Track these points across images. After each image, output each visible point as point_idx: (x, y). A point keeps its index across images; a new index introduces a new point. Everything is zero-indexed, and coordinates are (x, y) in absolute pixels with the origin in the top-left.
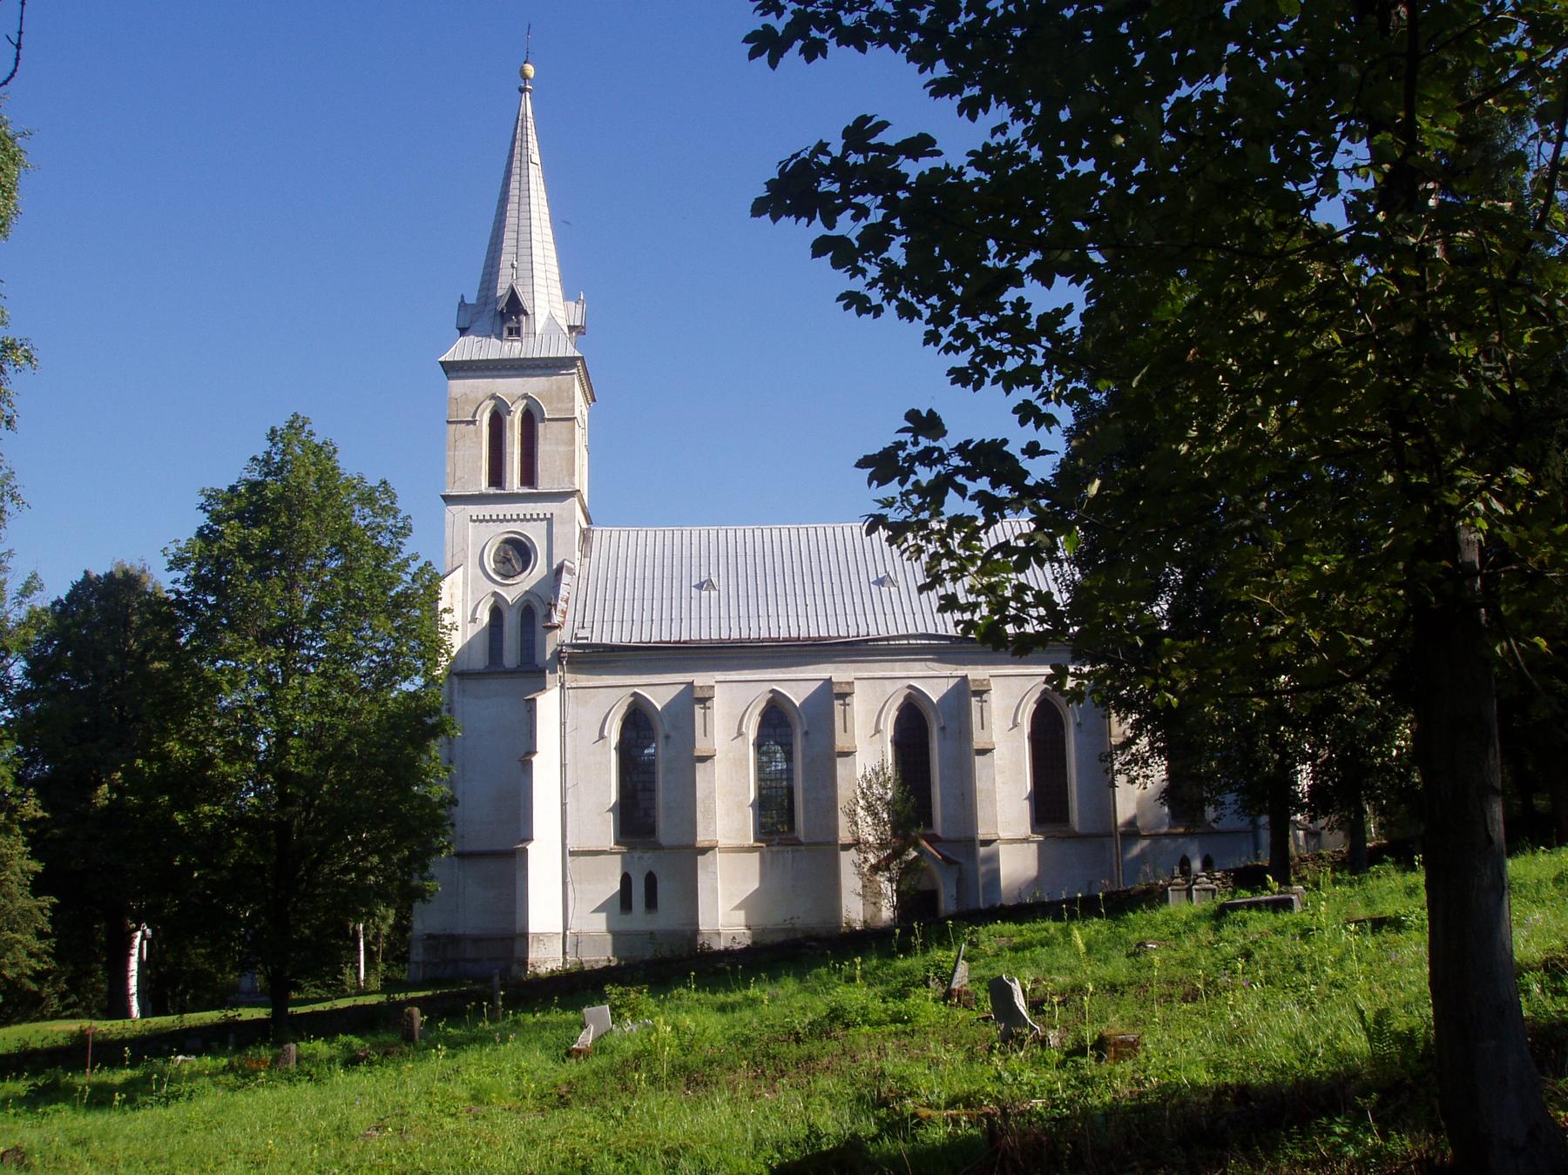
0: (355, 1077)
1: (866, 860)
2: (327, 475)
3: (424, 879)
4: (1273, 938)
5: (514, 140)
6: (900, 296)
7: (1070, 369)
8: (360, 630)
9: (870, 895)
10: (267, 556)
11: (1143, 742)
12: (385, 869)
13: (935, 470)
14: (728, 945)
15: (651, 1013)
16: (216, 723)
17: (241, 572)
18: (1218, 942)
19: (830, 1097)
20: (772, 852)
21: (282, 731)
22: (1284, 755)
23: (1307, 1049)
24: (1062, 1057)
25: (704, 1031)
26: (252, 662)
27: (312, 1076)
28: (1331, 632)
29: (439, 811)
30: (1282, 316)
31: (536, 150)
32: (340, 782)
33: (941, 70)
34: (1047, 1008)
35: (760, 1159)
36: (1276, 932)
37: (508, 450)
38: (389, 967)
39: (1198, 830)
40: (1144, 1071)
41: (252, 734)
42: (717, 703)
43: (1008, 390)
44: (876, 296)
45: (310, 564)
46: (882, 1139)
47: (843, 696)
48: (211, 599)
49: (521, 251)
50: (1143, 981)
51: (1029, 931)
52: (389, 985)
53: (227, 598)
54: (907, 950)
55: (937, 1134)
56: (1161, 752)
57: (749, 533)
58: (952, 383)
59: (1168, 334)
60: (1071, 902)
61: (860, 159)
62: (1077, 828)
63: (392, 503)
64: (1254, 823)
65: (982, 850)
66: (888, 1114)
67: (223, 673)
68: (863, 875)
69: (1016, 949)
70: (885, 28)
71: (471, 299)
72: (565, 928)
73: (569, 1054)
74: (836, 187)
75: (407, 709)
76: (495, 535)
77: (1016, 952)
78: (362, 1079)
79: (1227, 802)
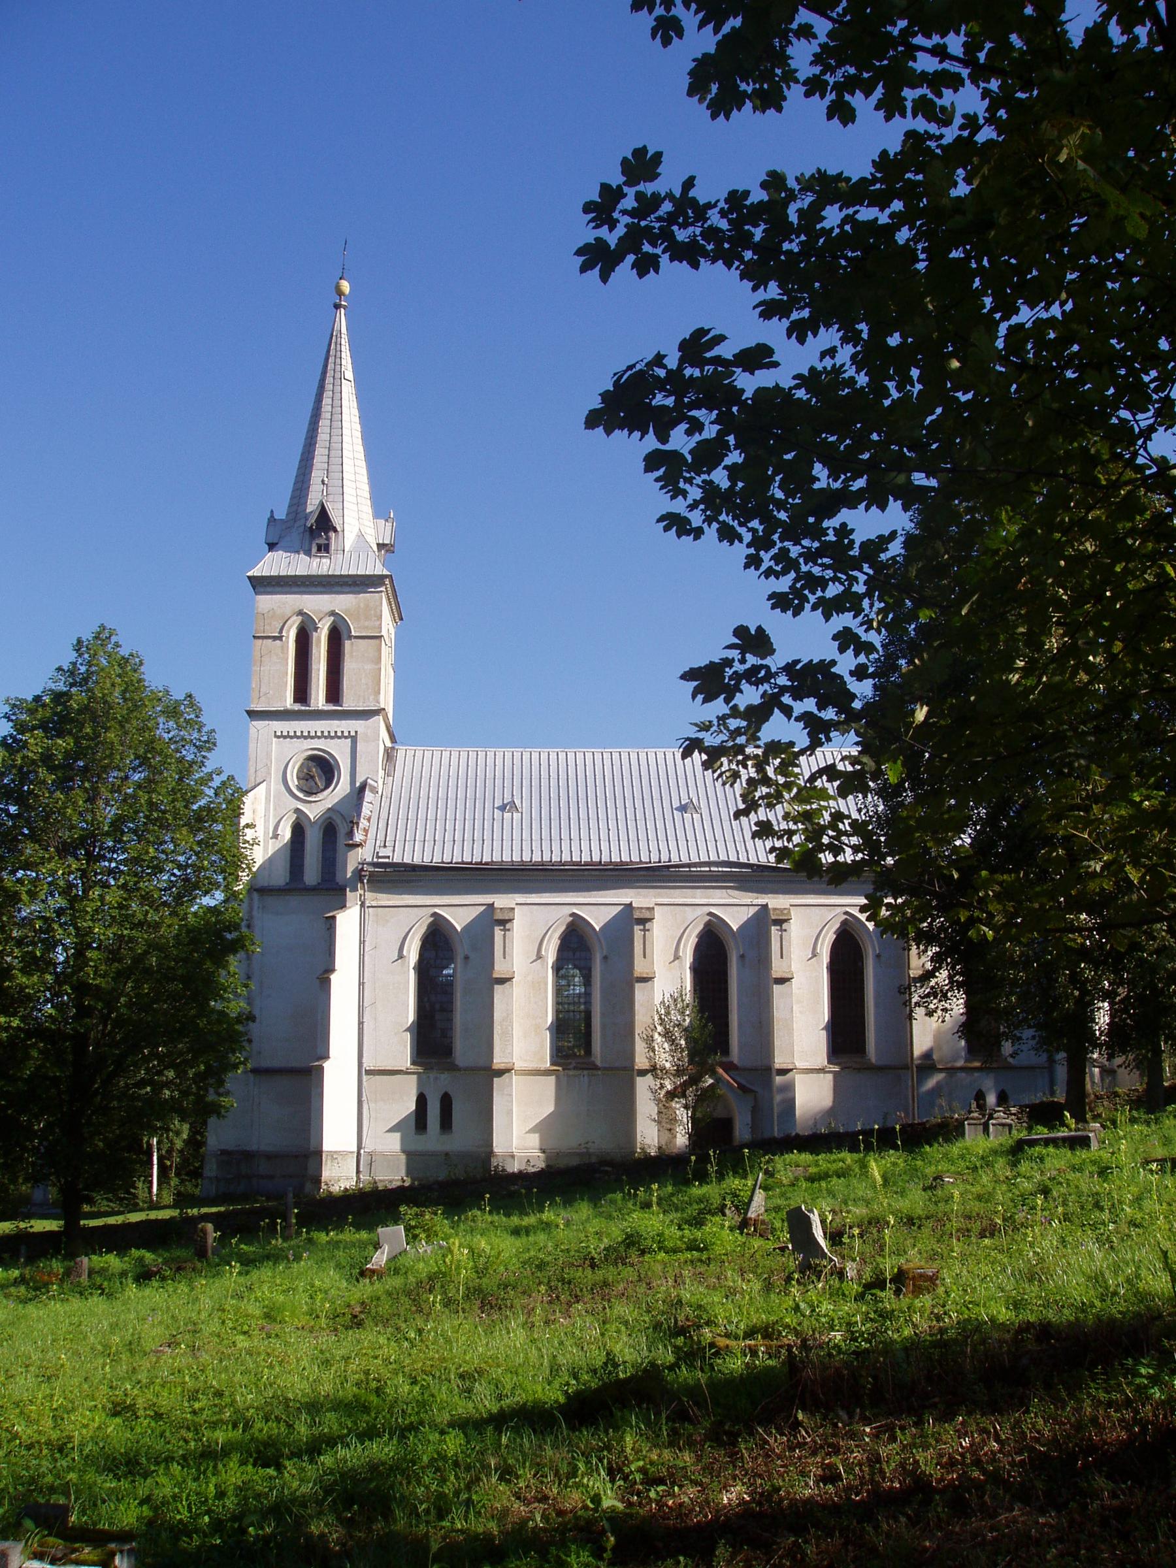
0: (147, 1291)
1: (662, 1086)
2: (133, 687)
3: (220, 1095)
4: (1071, 1176)
5: (328, 356)
6: (721, 518)
7: (891, 597)
8: (161, 844)
9: (665, 1121)
10: (70, 767)
11: (943, 976)
12: (181, 1084)
13: (762, 689)
14: (523, 1168)
15: (446, 1234)
16: (15, 934)
17: (44, 782)
18: (1015, 1177)
19: (626, 1323)
20: (568, 1076)
21: (81, 943)
22: (1084, 992)
23: (1107, 1288)
24: (860, 1289)
25: (499, 1254)
26: (53, 873)
27: (103, 1290)
28: (1150, 870)
29: (236, 1027)
30: (1114, 547)
31: (350, 367)
32: (137, 995)
33: (773, 291)
34: (845, 1240)
35: (556, 1384)
36: (1074, 1168)
37: (314, 667)
38: (182, 1182)
39: (995, 1065)
40: (944, 1306)
41: (51, 945)
42: (517, 925)
43: (827, 617)
44: (696, 518)
45: (113, 776)
46: (679, 1368)
47: (643, 921)
48: (13, 809)
49: (332, 468)
50: (940, 1215)
51: (824, 1161)
52: (182, 1200)
53: (29, 808)
54: (702, 1177)
55: (735, 1364)
56: (960, 985)
57: (553, 756)
58: (773, 608)
59: (999, 562)
60: (868, 1133)
61: (697, 373)
62: (873, 1060)
63: (197, 717)
64: (1051, 1061)
65: (778, 1079)
66: (685, 1343)
67: (22, 884)
68: (659, 1100)
69: (812, 1179)
70: (719, 245)
71: (281, 514)
72: (359, 1147)
73: (363, 1273)
74: (670, 401)
75: (207, 923)
76: (299, 751)
77: (813, 1182)
78: (153, 1294)
79: (1024, 1037)
